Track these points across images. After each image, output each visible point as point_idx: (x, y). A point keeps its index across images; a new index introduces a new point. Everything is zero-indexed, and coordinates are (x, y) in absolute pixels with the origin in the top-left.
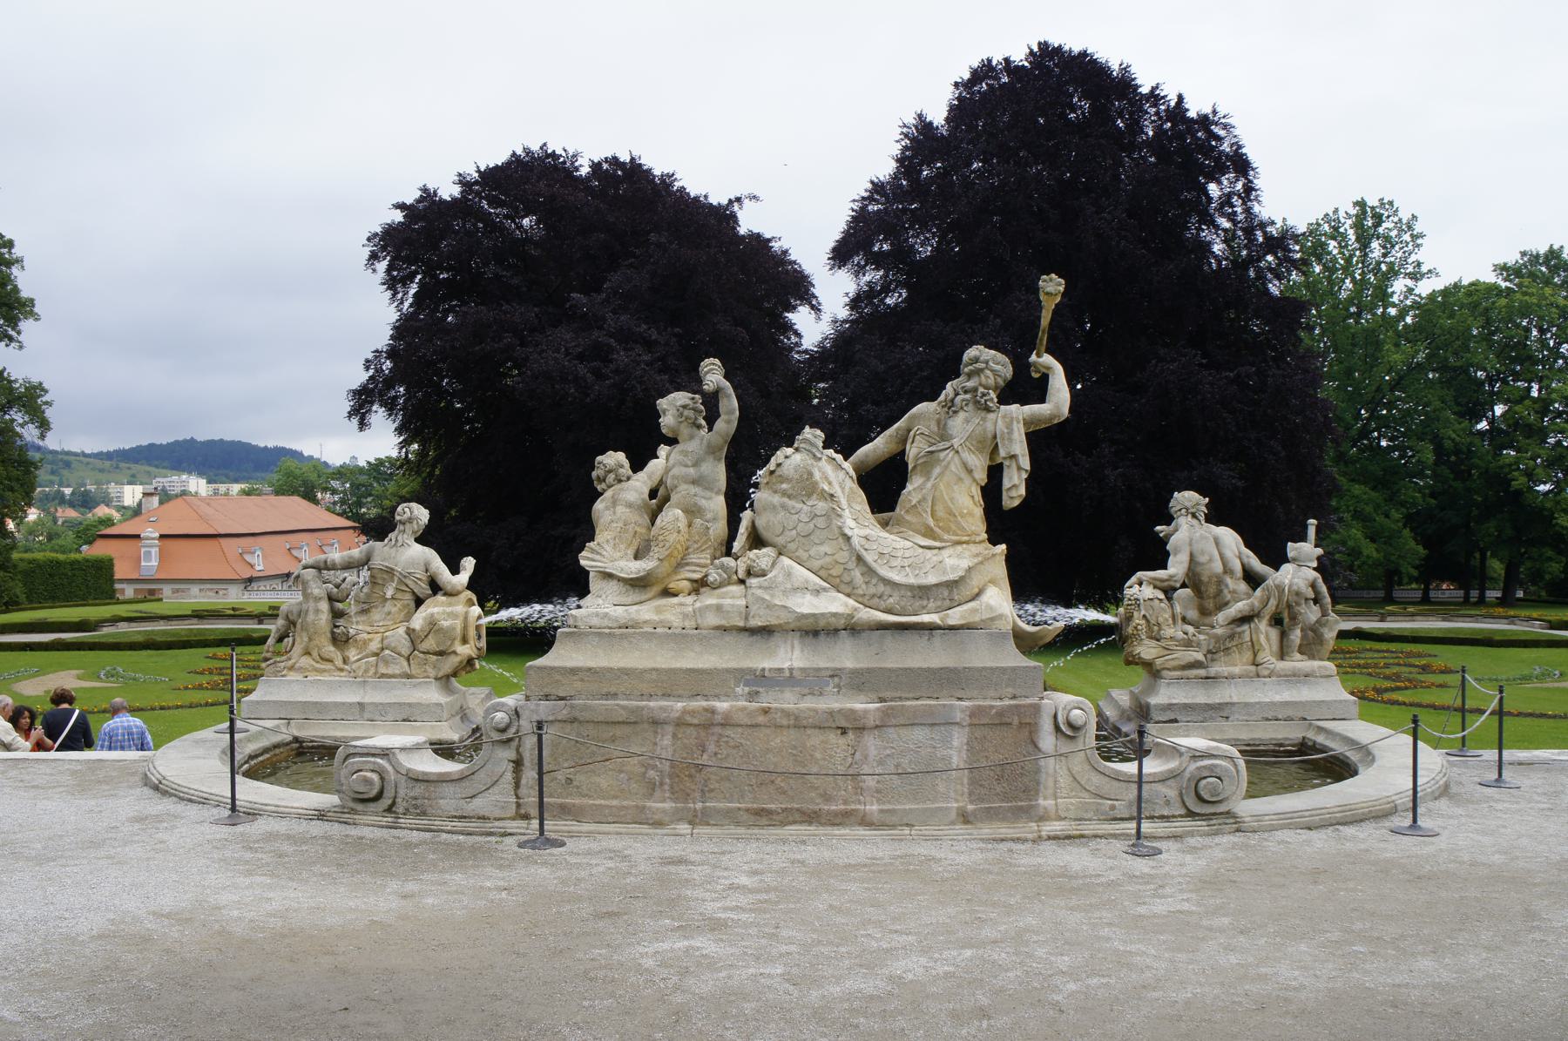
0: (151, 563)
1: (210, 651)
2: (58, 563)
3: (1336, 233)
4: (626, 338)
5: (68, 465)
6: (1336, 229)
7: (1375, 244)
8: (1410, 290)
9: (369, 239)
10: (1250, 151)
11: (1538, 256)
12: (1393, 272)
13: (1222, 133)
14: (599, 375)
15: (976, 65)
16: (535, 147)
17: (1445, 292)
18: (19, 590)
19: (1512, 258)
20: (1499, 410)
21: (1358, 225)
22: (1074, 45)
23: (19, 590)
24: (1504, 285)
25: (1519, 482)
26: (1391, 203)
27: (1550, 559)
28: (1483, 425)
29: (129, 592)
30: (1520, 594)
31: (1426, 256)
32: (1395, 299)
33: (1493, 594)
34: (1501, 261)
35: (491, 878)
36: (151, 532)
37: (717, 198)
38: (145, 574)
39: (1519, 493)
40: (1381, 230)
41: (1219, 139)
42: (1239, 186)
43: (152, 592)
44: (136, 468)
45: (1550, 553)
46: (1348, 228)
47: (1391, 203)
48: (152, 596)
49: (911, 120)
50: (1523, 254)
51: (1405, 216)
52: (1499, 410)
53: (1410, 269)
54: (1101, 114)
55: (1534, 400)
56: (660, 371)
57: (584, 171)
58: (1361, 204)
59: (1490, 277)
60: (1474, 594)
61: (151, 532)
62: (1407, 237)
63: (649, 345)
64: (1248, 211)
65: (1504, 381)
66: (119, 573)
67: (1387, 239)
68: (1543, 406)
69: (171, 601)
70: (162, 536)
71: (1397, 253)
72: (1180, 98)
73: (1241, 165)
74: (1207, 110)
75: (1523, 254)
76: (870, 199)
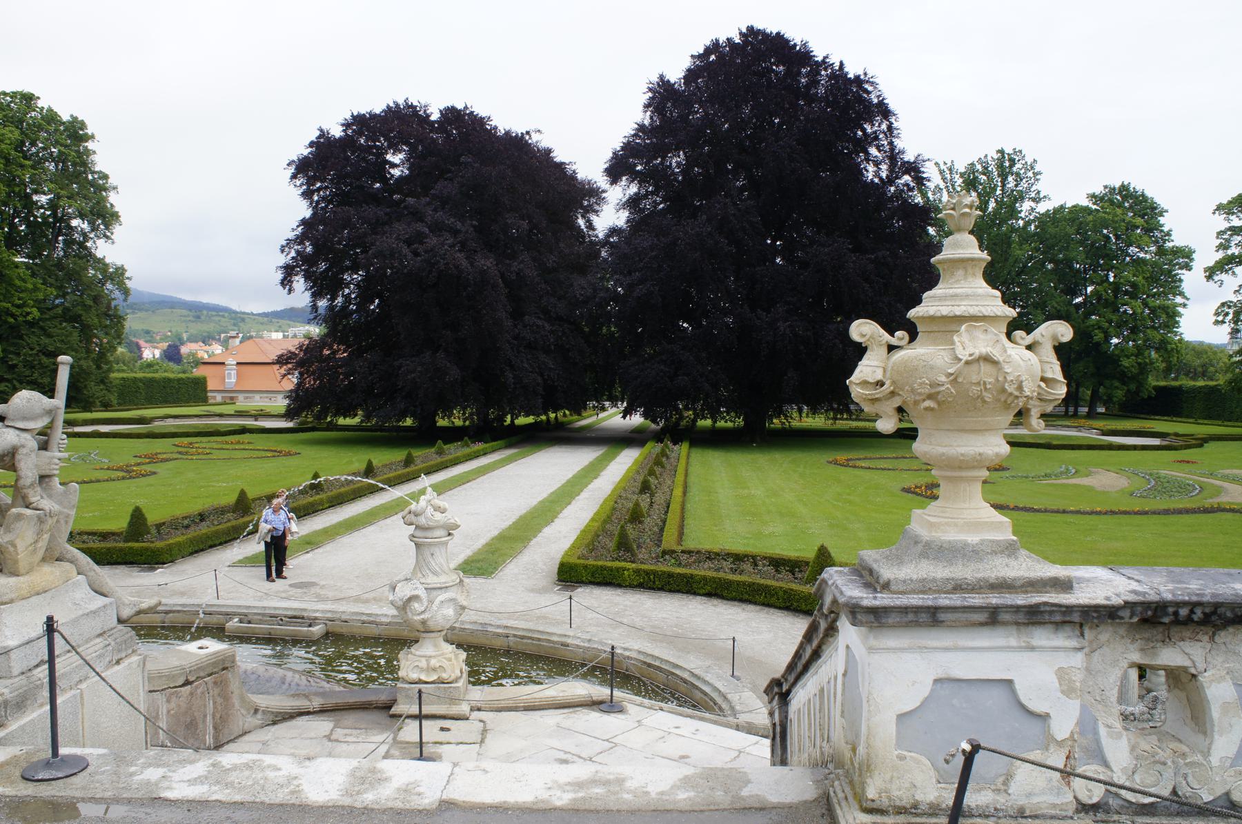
0: (231, 380)
1: (177, 441)
2: (169, 380)
3: (986, 171)
4: (437, 228)
5: (243, 320)
6: (986, 168)
7: (1010, 179)
8: (1033, 209)
9: (289, 165)
10: (892, 104)
11: (1114, 189)
12: (1021, 197)
13: (870, 88)
14: (416, 254)
15: (708, 43)
16: (401, 102)
17: (1056, 211)
18: (114, 399)
19: (1098, 190)
20: (1089, 289)
21: (1000, 165)
22: (772, 28)
23: (114, 399)
24: (1094, 207)
25: (1099, 336)
26: (1020, 151)
27: (1117, 388)
28: (1079, 300)
29: (219, 398)
30: (1101, 410)
31: (1042, 186)
32: (1022, 215)
33: (1084, 410)
34: (1091, 192)
35: (941, 450)
36: (231, 361)
38: (228, 387)
39: (1098, 344)
40: (1015, 169)
41: (868, 93)
42: (884, 127)
43: (232, 398)
44: (282, 322)
45: (1117, 384)
46: (992, 168)
47: (1020, 151)
48: (232, 401)
49: (655, 79)
50: (1106, 187)
51: (1029, 160)
52: (1089, 289)
53: (1033, 195)
54: (792, 74)
55: (1111, 284)
56: (460, 251)
57: (435, 116)
58: (1001, 152)
59: (1085, 202)
60: (1071, 409)
61: (231, 361)
62: (1030, 174)
63: (455, 232)
64: (891, 143)
65: (1094, 271)
67: (1018, 174)
68: (1116, 287)
69: (242, 404)
70: (238, 364)
71: (1024, 185)
72: (841, 64)
73: (884, 111)
74: (860, 72)
75: (1106, 187)
76: (635, 135)
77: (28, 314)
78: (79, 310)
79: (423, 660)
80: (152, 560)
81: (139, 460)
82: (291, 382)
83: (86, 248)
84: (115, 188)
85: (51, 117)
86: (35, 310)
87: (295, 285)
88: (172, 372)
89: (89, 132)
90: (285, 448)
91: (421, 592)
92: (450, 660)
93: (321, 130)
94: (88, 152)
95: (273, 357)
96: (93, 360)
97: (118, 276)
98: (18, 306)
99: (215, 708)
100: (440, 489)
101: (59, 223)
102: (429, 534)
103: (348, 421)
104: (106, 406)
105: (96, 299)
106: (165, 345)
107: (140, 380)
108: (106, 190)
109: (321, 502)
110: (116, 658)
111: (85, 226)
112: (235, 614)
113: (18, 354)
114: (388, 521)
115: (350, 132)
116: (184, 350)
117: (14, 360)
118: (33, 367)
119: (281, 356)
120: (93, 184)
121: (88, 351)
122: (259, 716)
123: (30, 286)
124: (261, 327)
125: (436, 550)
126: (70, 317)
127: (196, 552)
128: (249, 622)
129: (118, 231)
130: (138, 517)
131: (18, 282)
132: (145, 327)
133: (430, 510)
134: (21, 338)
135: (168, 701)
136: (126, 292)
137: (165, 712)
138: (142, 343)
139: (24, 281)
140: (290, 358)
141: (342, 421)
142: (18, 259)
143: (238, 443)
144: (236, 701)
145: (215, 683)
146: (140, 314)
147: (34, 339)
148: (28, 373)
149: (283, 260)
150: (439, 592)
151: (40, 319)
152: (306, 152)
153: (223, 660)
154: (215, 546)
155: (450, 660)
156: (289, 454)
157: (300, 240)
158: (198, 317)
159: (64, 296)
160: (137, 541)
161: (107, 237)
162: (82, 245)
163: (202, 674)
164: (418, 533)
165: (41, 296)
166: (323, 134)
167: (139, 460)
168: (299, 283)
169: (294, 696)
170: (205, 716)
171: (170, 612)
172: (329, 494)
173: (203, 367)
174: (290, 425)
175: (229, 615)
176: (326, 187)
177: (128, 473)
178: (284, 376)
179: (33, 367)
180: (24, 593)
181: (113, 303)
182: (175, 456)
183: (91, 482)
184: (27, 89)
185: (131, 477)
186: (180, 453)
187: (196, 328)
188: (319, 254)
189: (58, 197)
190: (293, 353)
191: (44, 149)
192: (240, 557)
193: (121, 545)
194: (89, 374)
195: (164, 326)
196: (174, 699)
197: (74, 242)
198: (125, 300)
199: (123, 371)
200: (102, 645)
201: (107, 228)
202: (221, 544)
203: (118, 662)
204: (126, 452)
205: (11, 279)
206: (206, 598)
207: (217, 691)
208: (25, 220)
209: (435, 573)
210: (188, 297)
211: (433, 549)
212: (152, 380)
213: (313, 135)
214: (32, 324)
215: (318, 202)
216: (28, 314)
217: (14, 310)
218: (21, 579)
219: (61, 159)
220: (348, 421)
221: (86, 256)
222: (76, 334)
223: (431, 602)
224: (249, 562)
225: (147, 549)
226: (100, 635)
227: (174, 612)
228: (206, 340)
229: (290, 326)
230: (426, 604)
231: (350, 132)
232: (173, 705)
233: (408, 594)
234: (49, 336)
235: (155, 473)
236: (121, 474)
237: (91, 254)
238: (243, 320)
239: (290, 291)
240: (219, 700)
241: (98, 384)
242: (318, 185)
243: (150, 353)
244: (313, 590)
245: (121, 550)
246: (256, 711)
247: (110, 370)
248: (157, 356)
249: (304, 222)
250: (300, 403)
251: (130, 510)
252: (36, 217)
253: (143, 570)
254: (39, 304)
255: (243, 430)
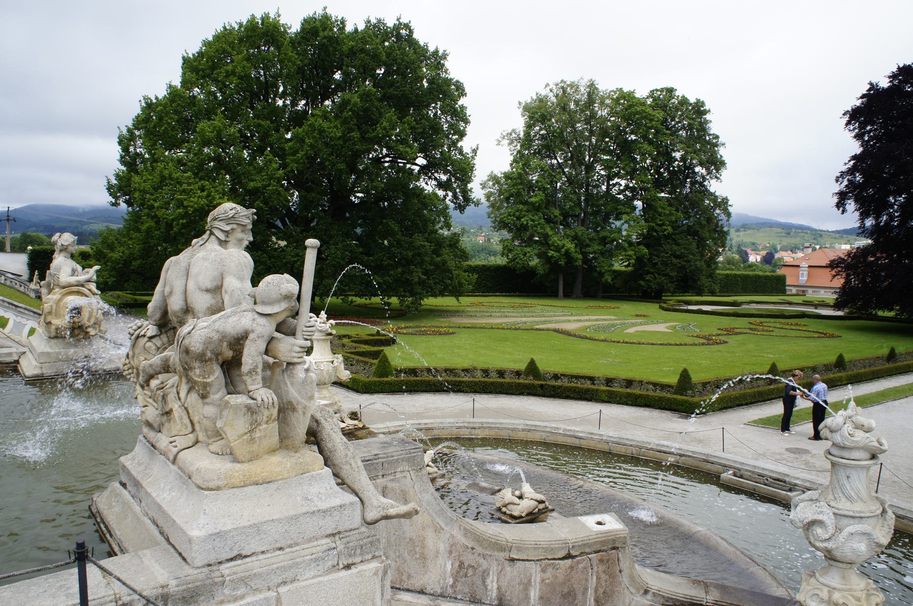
0: (803, 278)
1: (752, 320)
29: (794, 291)
36: (804, 265)
37: (320, 12)
43: (803, 291)
44: (850, 237)
48: (804, 293)
61: (804, 265)
66: (789, 281)
69: (811, 295)
77: (665, 230)
78: (697, 228)
79: (826, 590)
80: (685, 410)
81: (720, 332)
82: (839, 282)
83: (704, 186)
84: (723, 144)
85: (684, 101)
86: (669, 228)
87: (847, 207)
88: (767, 271)
89: (707, 108)
90: (830, 331)
91: (827, 517)
92: (858, 600)
93: (871, 84)
94: (706, 122)
95: (824, 262)
96: (705, 261)
97: (724, 204)
98: (660, 225)
99: (598, 583)
100: (862, 402)
101: (687, 170)
102: (846, 454)
103: (887, 314)
104: (713, 293)
105: (709, 220)
106: (764, 253)
107: (739, 276)
108: (717, 146)
109: (840, 379)
110: (344, 561)
111: (704, 171)
112: (731, 467)
113: (658, 257)
114: (897, 403)
115: (896, 82)
116: (777, 256)
117: (656, 260)
118: (667, 265)
119: (832, 261)
120: (709, 143)
121: (702, 255)
122: (649, 597)
123: (667, 212)
124: (834, 241)
125: (854, 474)
126: (691, 232)
127: (726, 408)
128: (741, 477)
129: (724, 173)
130: (685, 376)
131: (660, 210)
132: (752, 240)
133: (848, 428)
134: (660, 245)
135: (543, 571)
136: (729, 215)
137: (538, 580)
138: (749, 251)
139: (663, 208)
140: (840, 263)
141: (880, 313)
142: (663, 195)
143: (797, 324)
144: (625, 579)
145: (601, 561)
146: (749, 232)
147: (668, 246)
148: (664, 268)
149: (837, 188)
150: (851, 521)
151: (673, 234)
152: (858, 103)
153: (614, 541)
154: (742, 405)
155: (858, 600)
156: (832, 336)
157: (851, 171)
158: (789, 234)
159: (688, 218)
160: (682, 395)
161: (718, 178)
162: (701, 184)
163: (587, 550)
164: (834, 451)
165: (673, 218)
166: (873, 86)
167: (720, 332)
168: (851, 205)
169: (696, 582)
170: (586, 589)
171: (683, 455)
172: (850, 373)
173: (784, 268)
174: (840, 313)
175: (726, 467)
176: (876, 130)
177: (709, 340)
178: (834, 276)
179: (667, 265)
180: (236, 481)
181: (720, 223)
182: (745, 331)
183: (681, 345)
184: (669, 85)
185: (708, 344)
186: (751, 329)
187: (786, 241)
188: (865, 184)
189: (687, 153)
190: (843, 259)
191: (679, 122)
192: (756, 418)
193: (669, 395)
194: (702, 270)
195: (765, 240)
196: (550, 570)
197: (696, 182)
198: (728, 220)
199: (732, 270)
200: (325, 547)
201: (717, 172)
202: (747, 404)
203: (348, 567)
204: (712, 325)
205: (656, 208)
206: (713, 450)
207: (602, 568)
208: (667, 169)
209: (849, 499)
210: (782, 220)
211: (848, 471)
212: (747, 276)
213: (864, 89)
214: (668, 237)
215: (868, 141)
216: (665, 230)
217: (657, 228)
218: (238, 466)
219: (690, 127)
220: (887, 314)
221: (703, 191)
222: (694, 244)
223: (838, 529)
224: (765, 423)
225: (686, 401)
226: (334, 535)
227: (686, 456)
228: (793, 249)
229: (856, 240)
230: (831, 530)
231: (896, 82)
232: (549, 574)
233: (810, 516)
234: (678, 245)
235: (726, 342)
236: (702, 341)
237: (707, 190)
238: (821, 236)
239: (843, 212)
240: (604, 577)
241: (707, 277)
242: (869, 128)
243: (754, 258)
244: (804, 457)
245: (668, 399)
246: (646, 592)
247: (717, 268)
248: (759, 260)
249: (854, 157)
250: (845, 298)
251: (682, 369)
252: (674, 167)
253: (681, 417)
254: (674, 224)
255: (803, 315)
